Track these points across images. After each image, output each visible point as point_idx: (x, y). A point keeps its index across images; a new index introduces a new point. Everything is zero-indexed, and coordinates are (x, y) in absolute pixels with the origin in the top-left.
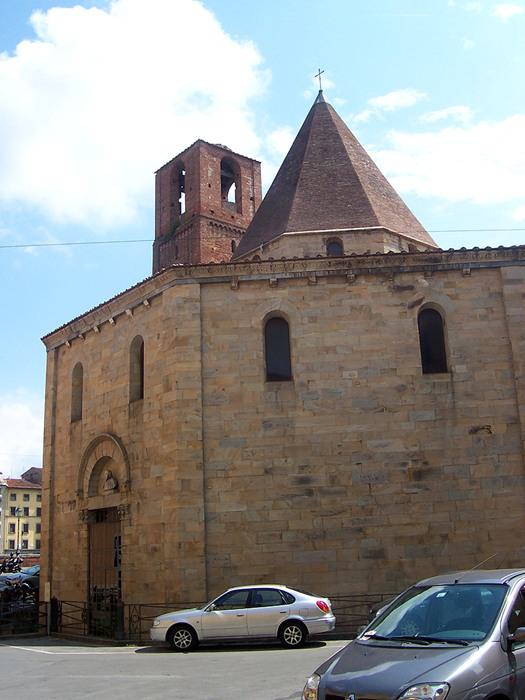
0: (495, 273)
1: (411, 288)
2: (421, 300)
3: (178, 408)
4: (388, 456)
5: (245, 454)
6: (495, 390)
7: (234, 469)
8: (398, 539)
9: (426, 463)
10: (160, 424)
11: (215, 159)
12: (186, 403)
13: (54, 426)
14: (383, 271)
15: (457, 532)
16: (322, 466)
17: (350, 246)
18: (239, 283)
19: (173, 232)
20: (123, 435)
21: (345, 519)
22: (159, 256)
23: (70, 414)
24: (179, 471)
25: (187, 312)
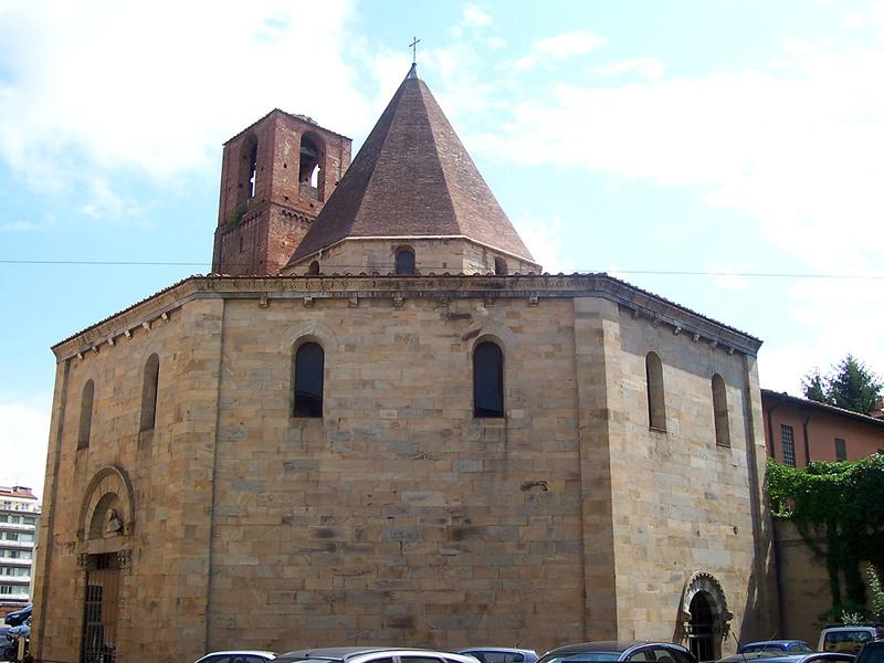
0: (569, 303)
1: (467, 316)
2: (478, 332)
3: (188, 441)
4: (425, 510)
5: (261, 500)
6: (555, 440)
7: (247, 516)
8: (428, 607)
9: (468, 521)
10: (167, 459)
11: (295, 134)
12: (197, 437)
13: (58, 453)
14: (435, 295)
15: (498, 602)
16: (348, 518)
17: (426, 260)
18: (269, 300)
19: (239, 218)
20: (130, 469)
21: (370, 580)
22: (221, 247)
23: (77, 439)
24: (184, 514)
25: (206, 332)
